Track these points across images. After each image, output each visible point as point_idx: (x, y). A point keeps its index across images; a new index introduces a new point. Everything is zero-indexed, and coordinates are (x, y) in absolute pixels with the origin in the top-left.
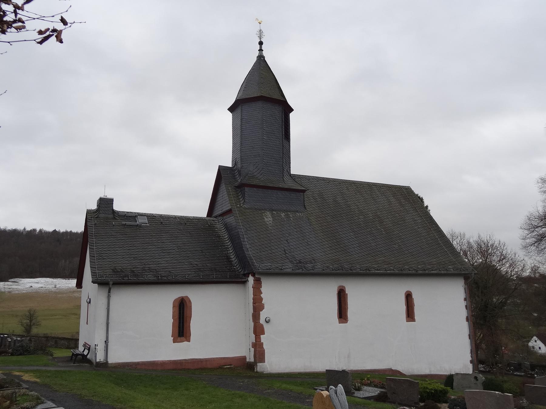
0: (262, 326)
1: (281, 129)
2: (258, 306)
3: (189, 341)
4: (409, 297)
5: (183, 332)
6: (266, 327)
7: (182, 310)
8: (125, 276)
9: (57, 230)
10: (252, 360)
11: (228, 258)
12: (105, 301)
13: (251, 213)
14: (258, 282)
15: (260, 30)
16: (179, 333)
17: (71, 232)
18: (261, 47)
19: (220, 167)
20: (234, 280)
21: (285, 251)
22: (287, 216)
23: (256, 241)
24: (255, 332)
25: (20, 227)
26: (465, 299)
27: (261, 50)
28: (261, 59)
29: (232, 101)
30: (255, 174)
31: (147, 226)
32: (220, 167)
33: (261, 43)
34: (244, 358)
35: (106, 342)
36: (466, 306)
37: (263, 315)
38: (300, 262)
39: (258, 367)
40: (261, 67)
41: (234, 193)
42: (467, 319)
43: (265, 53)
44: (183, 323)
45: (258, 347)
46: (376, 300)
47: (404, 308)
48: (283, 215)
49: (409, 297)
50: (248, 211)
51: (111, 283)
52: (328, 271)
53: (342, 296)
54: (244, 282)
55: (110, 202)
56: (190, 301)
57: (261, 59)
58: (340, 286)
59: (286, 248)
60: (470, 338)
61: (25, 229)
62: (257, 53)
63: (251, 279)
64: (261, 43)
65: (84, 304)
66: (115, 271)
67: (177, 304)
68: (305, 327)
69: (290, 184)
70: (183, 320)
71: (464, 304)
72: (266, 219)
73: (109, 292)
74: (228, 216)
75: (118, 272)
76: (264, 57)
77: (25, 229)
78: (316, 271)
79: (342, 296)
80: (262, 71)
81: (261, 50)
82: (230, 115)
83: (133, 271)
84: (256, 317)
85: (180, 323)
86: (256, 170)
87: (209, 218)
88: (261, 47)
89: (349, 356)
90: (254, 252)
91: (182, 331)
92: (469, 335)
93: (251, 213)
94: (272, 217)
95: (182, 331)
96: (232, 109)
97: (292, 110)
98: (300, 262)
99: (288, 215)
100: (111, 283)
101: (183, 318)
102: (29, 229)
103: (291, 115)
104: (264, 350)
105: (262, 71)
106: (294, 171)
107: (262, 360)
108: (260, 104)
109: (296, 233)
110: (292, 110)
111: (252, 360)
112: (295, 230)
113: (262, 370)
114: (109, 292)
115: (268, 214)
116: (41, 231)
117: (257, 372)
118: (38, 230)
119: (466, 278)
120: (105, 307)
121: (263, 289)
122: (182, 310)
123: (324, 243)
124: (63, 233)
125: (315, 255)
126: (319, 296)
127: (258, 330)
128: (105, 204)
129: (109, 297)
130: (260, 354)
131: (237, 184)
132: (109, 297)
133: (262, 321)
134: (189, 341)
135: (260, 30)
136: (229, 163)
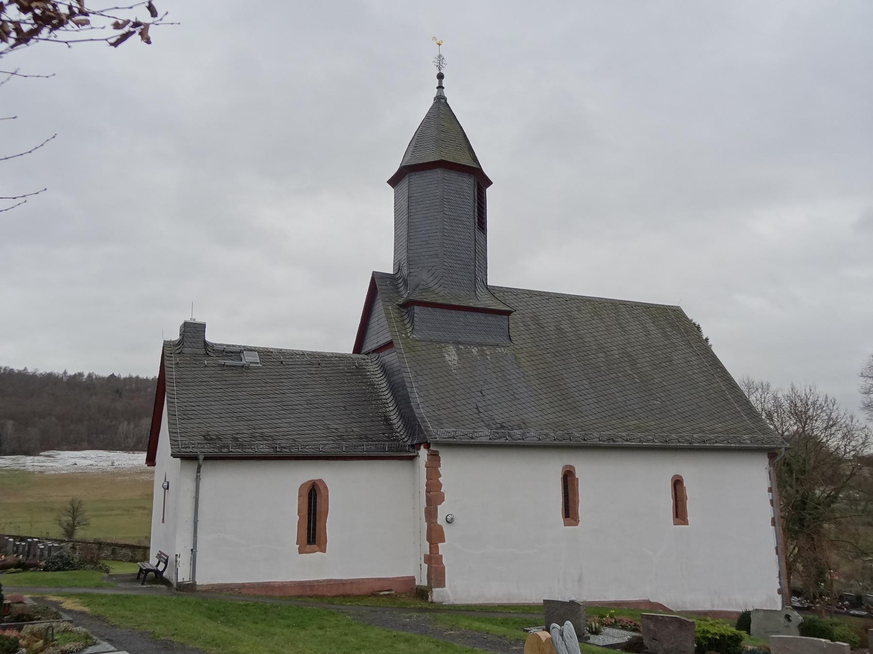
0: (441, 528)
1: (472, 213)
2: (434, 496)
3: (324, 551)
5: (314, 537)
6: (447, 530)
7: (313, 499)
9: (116, 374)
10: (425, 583)
11: (387, 420)
14: (434, 457)
15: (440, 56)
16: (309, 537)
17: (137, 377)
18: (440, 82)
20: (396, 454)
21: (477, 408)
22: (482, 354)
24: (429, 539)
26: (770, 490)
27: (440, 87)
28: (441, 101)
31: (259, 368)
33: (440, 77)
34: (413, 579)
35: (193, 551)
37: (443, 511)
38: (502, 427)
39: (435, 594)
40: (440, 105)
41: (396, 315)
43: (446, 93)
44: (315, 522)
45: (433, 561)
46: (623, 488)
47: (671, 502)
48: (475, 350)
49: (569, 479)
51: (201, 457)
55: (199, 329)
56: (326, 487)
57: (441, 101)
58: (566, 466)
59: (479, 404)
60: (777, 553)
61: (65, 373)
62: (434, 92)
63: (423, 453)
64: (440, 77)
66: (207, 438)
67: (306, 493)
68: (505, 529)
71: (768, 496)
72: (448, 358)
73: (198, 471)
74: (387, 352)
75: (212, 439)
77: (65, 373)
79: (569, 479)
80: (441, 118)
81: (440, 87)
82: (391, 190)
83: (236, 439)
84: (431, 513)
87: (357, 355)
89: (580, 580)
91: (312, 534)
92: (777, 548)
95: (312, 534)
96: (394, 182)
97: (489, 183)
98: (502, 427)
99: (483, 350)
100: (201, 457)
101: (315, 514)
102: (71, 372)
103: (489, 191)
104: (444, 568)
105: (441, 118)
107: (441, 584)
108: (438, 174)
110: (489, 183)
111: (425, 583)
113: (440, 600)
114: (198, 471)
115: (451, 348)
116: (90, 376)
117: (432, 602)
118: (86, 374)
119: (772, 454)
122: (313, 499)
124: (125, 379)
127: (435, 536)
128: (193, 331)
129: (198, 479)
130: (437, 574)
131: (401, 301)
132: (198, 479)
133: (441, 520)
134: (324, 551)
135: (440, 56)
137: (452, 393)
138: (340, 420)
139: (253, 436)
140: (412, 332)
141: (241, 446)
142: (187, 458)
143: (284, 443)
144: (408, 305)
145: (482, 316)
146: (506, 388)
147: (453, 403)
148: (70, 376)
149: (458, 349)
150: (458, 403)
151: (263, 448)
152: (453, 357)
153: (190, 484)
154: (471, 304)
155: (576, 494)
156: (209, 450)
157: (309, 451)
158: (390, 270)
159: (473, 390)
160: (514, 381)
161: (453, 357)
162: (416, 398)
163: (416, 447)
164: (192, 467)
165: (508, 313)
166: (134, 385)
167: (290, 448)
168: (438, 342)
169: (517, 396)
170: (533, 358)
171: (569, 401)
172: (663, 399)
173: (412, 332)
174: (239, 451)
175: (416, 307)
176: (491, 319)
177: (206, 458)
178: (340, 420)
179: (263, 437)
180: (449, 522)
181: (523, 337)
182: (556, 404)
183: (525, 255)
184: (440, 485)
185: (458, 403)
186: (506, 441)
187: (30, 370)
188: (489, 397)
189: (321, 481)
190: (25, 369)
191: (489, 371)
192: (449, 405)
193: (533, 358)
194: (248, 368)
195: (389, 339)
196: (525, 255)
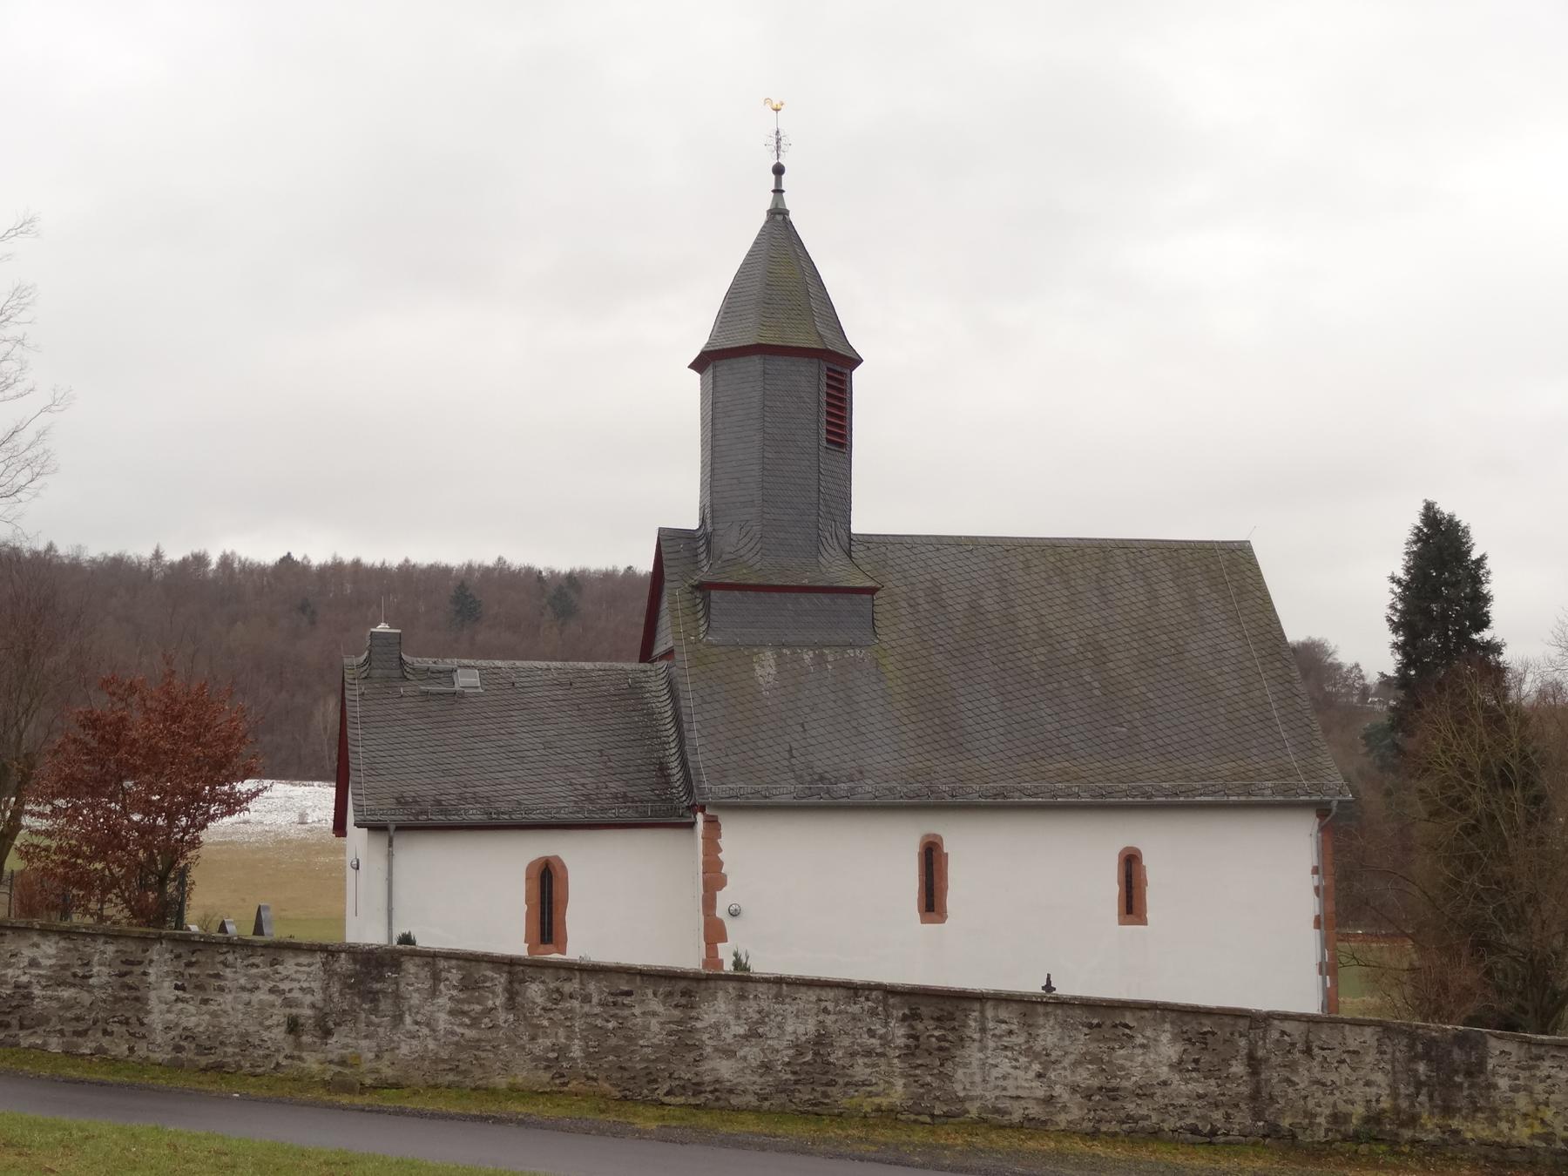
0: (721, 923)
1: (814, 426)
2: (714, 879)
4: (1131, 865)
5: (550, 933)
6: (731, 926)
8: (422, 813)
9: (297, 557)
11: (663, 768)
12: (383, 864)
13: (723, 657)
14: (712, 823)
16: (542, 934)
17: (357, 564)
18: (778, 182)
19: (661, 530)
20: (661, 820)
21: (790, 751)
22: (820, 660)
23: (721, 728)
25: (139, 550)
26: (1315, 871)
27: (778, 191)
28: (778, 217)
29: (694, 354)
30: (742, 552)
31: (478, 695)
32: (661, 530)
33: (779, 170)
36: (1317, 889)
37: (724, 900)
38: (822, 779)
41: (686, 604)
42: (1318, 923)
43: (789, 201)
44: (550, 913)
48: (808, 656)
49: (1131, 865)
50: (715, 650)
51: (392, 827)
52: (889, 800)
53: (932, 860)
54: (692, 825)
56: (563, 867)
57: (778, 217)
58: (928, 836)
59: (794, 745)
61: (158, 555)
62: (767, 201)
63: (700, 817)
64: (779, 170)
65: (350, 872)
66: (401, 801)
67: (536, 874)
69: (838, 571)
70: (550, 910)
71: (1313, 881)
72: (759, 671)
73: (390, 845)
75: (407, 803)
76: (785, 213)
77: (158, 555)
78: (856, 799)
79: (932, 860)
80: (780, 273)
81: (778, 191)
82: (695, 377)
83: (439, 803)
84: (709, 903)
85: (543, 913)
86: (746, 540)
88: (778, 182)
90: (710, 755)
93: (723, 657)
94: (778, 665)
96: (699, 364)
97: (857, 361)
98: (822, 779)
99: (822, 655)
100: (392, 827)
101: (550, 903)
102: (174, 554)
103: (858, 375)
106: (866, 518)
108: (755, 363)
109: (832, 705)
110: (857, 361)
112: (832, 696)
114: (390, 845)
115: (769, 656)
116: (226, 562)
118: (214, 559)
119: (1322, 810)
120: (383, 875)
121: (723, 842)
123: (903, 728)
124: (324, 570)
125: (869, 760)
126: (883, 855)
129: (390, 856)
131: (697, 578)
132: (390, 856)
133: (721, 912)
136: (689, 519)
137: (754, 729)
138: (591, 771)
139: (461, 797)
140: (707, 633)
141: (445, 812)
142: (375, 828)
143: (504, 807)
144: (704, 588)
145: (825, 599)
146: (846, 717)
147: (752, 745)
148: (172, 566)
149: (780, 656)
150: (760, 743)
151: (476, 816)
152: (769, 670)
153: (382, 864)
154: (806, 582)
155: (944, 877)
156: (401, 818)
157: (536, 817)
158: (693, 524)
159: (790, 722)
160: (864, 705)
161: (769, 670)
162: (695, 738)
163: (694, 809)
164: (382, 841)
165: (872, 591)
166: (348, 588)
167: (510, 813)
168: (748, 646)
169: (863, 729)
170: (909, 664)
171: (953, 734)
172: (1137, 723)
173: (707, 633)
174: (439, 819)
175: (712, 592)
176: (842, 601)
177: (401, 828)
178: (591, 771)
179: (476, 798)
180: (734, 914)
181: (902, 627)
182: (928, 739)
183: (913, 473)
184: (720, 864)
185: (760, 743)
186: (824, 797)
187: (64, 549)
188: (814, 733)
189: (557, 858)
190: (51, 547)
191: (825, 690)
192: (744, 748)
193: (909, 664)
194: (462, 695)
195: (670, 644)
196: (913, 473)
